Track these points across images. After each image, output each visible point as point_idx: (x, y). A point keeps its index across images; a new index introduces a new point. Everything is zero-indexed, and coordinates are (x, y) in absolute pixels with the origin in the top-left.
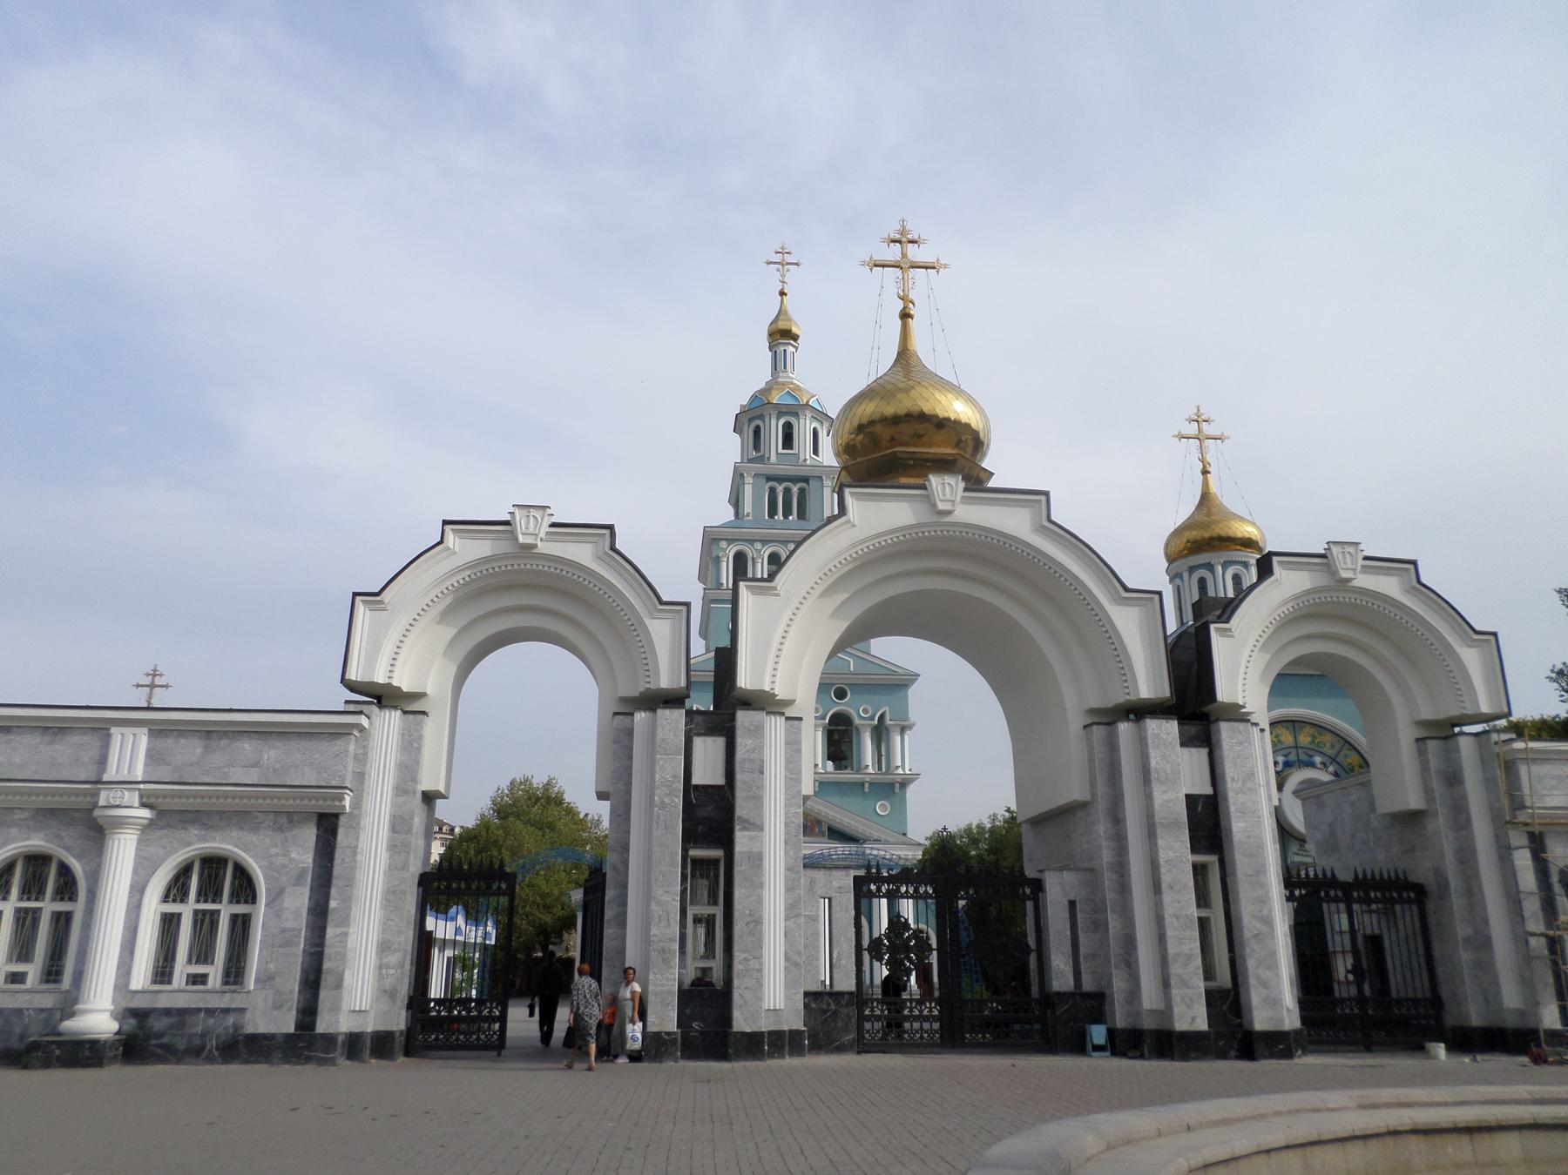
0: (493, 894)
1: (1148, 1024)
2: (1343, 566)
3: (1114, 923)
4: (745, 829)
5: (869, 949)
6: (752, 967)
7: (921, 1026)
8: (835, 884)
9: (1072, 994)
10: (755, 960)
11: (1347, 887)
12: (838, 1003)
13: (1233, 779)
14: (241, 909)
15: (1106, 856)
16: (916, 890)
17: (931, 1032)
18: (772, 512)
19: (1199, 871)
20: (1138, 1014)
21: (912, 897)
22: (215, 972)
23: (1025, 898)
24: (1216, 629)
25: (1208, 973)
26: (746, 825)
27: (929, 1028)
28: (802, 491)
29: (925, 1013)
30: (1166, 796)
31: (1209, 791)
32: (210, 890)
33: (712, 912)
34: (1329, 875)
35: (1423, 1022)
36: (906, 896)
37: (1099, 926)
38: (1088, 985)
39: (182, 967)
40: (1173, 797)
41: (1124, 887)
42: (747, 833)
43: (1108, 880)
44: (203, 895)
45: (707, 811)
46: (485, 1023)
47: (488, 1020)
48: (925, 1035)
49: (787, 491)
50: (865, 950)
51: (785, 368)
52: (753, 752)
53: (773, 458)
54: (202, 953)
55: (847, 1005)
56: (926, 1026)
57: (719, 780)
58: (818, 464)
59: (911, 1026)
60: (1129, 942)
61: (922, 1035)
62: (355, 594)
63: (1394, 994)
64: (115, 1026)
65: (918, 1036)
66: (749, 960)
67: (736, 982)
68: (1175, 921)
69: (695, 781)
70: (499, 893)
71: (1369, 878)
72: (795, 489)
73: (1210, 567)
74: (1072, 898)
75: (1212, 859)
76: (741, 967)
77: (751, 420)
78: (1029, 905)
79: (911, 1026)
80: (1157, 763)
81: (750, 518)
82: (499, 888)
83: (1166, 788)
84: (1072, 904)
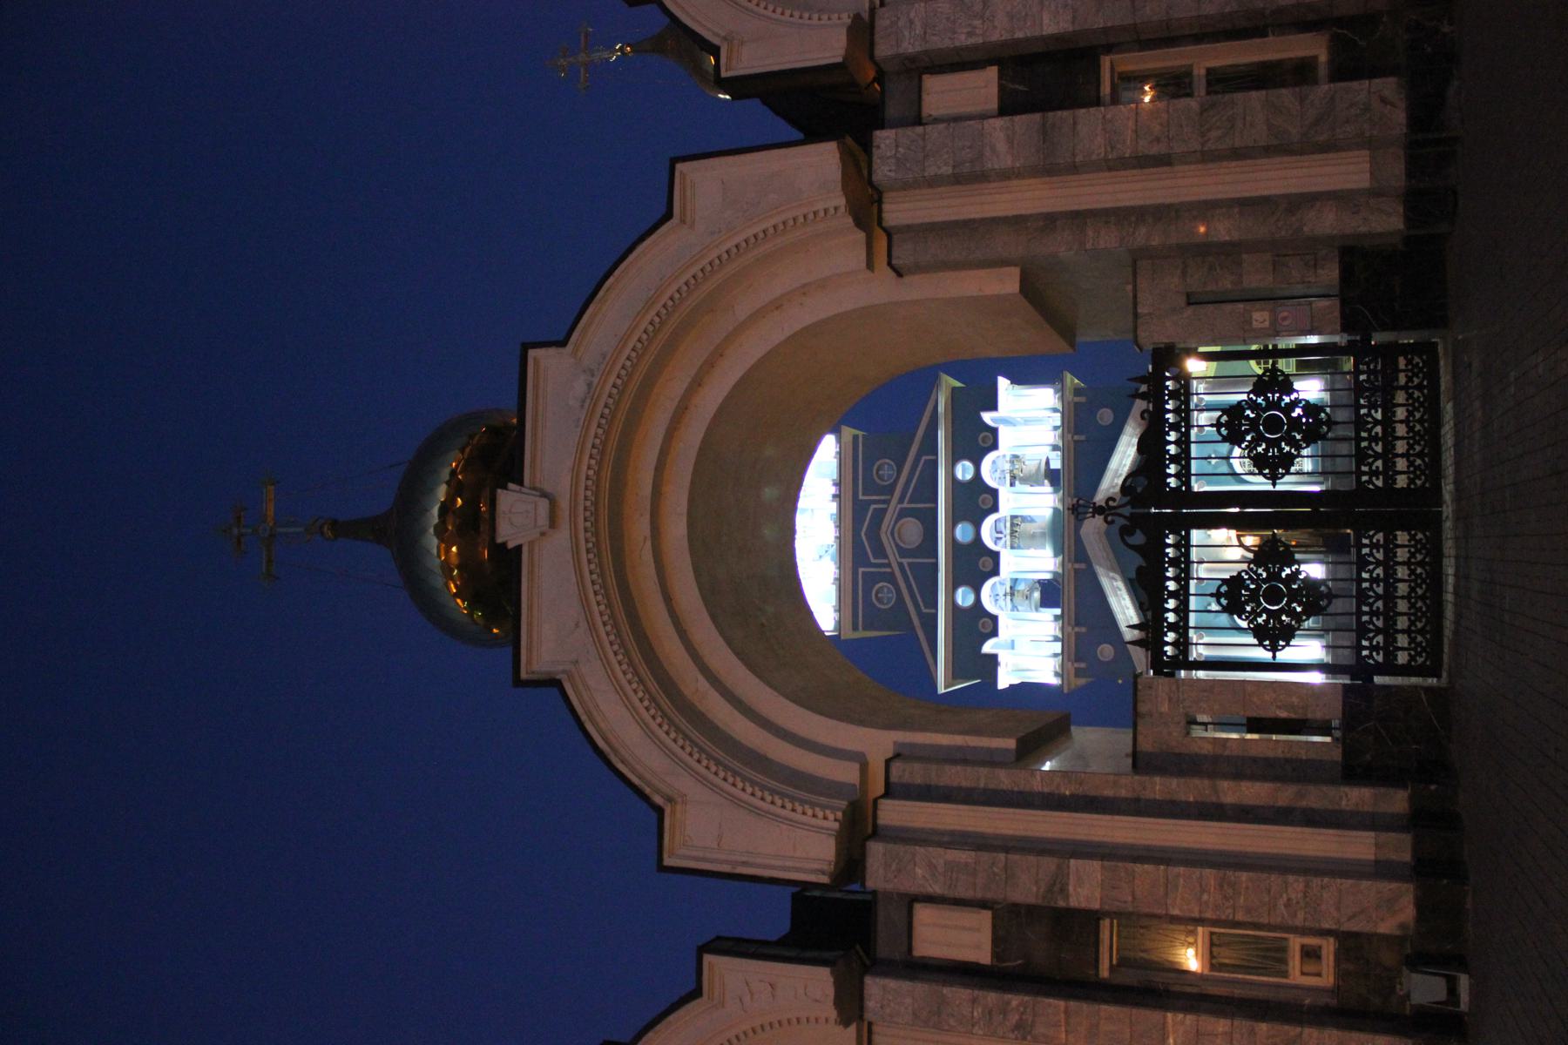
1: (1396, 171)
4: (1063, 890)
6: (1300, 895)
7: (1402, 456)
8: (1165, 708)
9: (1343, 303)
10: (1290, 890)
13: (970, 34)
15: (1107, 239)
17: (1416, 548)
20: (1375, 193)
24: (727, 70)
25: (1300, 73)
26: (1056, 889)
27: (1405, 618)
29: (1380, 623)
30: (1002, 147)
31: (992, 72)
35: (1402, 588)
37: (1229, 253)
38: (1330, 274)
40: (1002, 135)
42: (1071, 888)
43: (1145, 236)
46: (1396, 589)
47: (1392, 617)
48: (1416, 381)
50: (1274, 657)
52: (935, 867)
56: (1402, 555)
57: (986, 916)
59: (1402, 438)
61: (1415, 387)
65: (1417, 394)
66: (1289, 900)
68: (1214, 134)
71: (1128, 523)
74: (1182, 301)
76: (1301, 915)
79: (1402, 438)
80: (946, 164)
83: (988, 148)
84: (1192, 300)
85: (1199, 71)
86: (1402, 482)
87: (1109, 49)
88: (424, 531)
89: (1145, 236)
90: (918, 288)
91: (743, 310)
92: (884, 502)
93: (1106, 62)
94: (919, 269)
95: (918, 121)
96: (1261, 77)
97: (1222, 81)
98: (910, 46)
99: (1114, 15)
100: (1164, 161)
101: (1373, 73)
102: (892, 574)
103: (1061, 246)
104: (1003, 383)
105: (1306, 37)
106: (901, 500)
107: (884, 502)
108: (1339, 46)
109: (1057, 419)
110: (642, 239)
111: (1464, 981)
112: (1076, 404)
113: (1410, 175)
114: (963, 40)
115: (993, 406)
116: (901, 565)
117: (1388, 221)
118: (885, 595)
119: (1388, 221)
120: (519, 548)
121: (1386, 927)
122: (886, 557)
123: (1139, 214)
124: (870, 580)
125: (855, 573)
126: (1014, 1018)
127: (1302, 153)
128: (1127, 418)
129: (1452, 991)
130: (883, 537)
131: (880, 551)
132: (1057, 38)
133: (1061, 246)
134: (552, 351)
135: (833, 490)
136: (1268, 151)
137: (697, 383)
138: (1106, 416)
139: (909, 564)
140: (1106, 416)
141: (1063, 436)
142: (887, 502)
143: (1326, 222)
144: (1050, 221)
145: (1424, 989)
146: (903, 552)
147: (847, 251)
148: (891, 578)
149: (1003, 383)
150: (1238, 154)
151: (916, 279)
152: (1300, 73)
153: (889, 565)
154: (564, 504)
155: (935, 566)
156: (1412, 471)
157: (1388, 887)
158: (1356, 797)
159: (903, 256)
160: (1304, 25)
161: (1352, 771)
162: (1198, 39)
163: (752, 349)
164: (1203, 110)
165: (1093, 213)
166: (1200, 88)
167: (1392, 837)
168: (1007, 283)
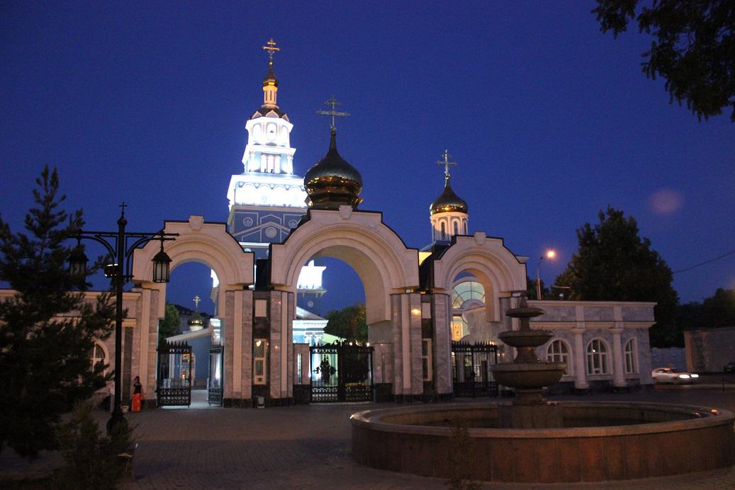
1: (406, 393)
3: (397, 361)
4: (274, 332)
11: (472, 347)
14: (604, 353)
15: (396, 339)
16: (175, 351)
17: (334, 397)
19: (424, 344)
20: (402, 389)
21: (174, 353)
22: (601, 369)
23: (368, 353)
32: (556, 350)
34: (185, 344)
35: (176, 398)
36: (172, 353)
37: (392, 362)
38: (387, 381)
39: (594, 370)
41: (401, 350)
43: (396, 345)
45: (260, 326)
54: (597, 365)
56: (333, 395)
60: (402, 366)
63: (489, 381)
64: (588, 385)
67: (271, 383)
69: (256, 315)
70: (186, 353)
75: (429, 340)
78: (369, 355)
85: (427, 357)
86: (314, 396)
87: (433, 340)
88: (335, 172)
89: (396, 345)
90: (388, 299)
91: (385, 260)
92: (282, 223)
93: (430, 340)
94: (392, 300)
95: (422, 302)
96: (425, 369)
97: (425, 361)
98: (437, 302)
99: (438, 342)
100: (411, 351)
101: (424, 390)
102: (256, 226)
103: (395, 330)
104: (324, 268)
105: (431, 377)
106: (283, 230)
107: (282, 223)
108: (429, 383)
109: (310, 288)
110: (402, 241)
111: (263, 407)
112: (315, 294)
113: (406, 395)
114: (436, 312)
115: (316, 264)
116: (259, 229)
117: (397, 392)
118: (248, 222)
119: (397, 392)
120: (338, 210)
121: (272, 393)
122: (263, 223)
123: (401, 346)
124: (254, 217)
125: (257, 211)
126: (247, 322)
127: (411, 376)
128: (310, 311)
129: (261, 405)
130: (270, 223)
131: (265, 221)
132: (435, 330)
133: (395, 330)
134: (380, 219)
135: (287, 205)
136: (411, 370)
137: (370, 248)
138: (311, 304)
139: (259, 233)
140: (311, 304)
141: (304, 290)
142: (282, 225)
143: (397, 380)
144: (400, 328)
145: (261, 400)
146: (264, 230)
147: (396, 283)
148: (254, 225)
149: (324, 268)
150: (411, 365)
151: (389, 299)
152: (425, 376)
153: (259, 225)
154: (349, 221)
155: (258, 242)
156: (315, 398)
157: (279, 393)
158: (291, 388)
159: (395, 297)
160: (434, 377)
161: (295, 386)
162: (433, 357)
163: (377, 262)
164: (420, 359)
165: (401, 336)
166: (424, 357)
167: (286, 394)
168: (388, 317)
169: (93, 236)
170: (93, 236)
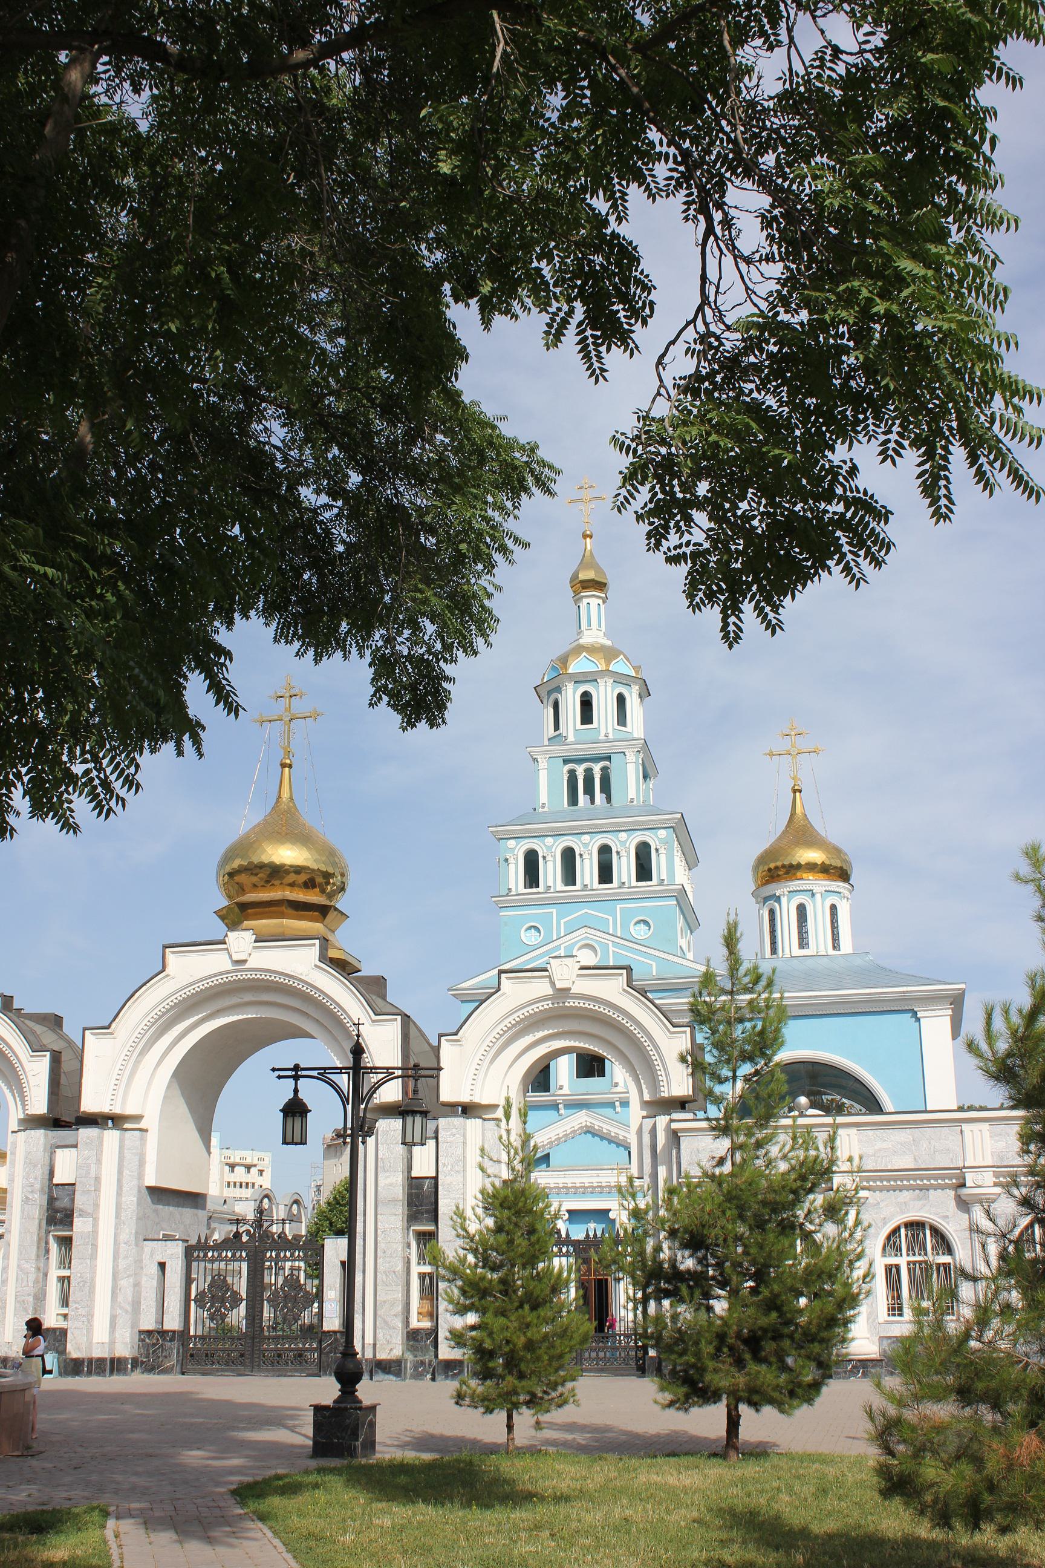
0: (237, 1260)
2: (560, 977)
5: (196, 1301)
8: (169, 1252)
12: (164, 1340)
18: (573, 800)
28: (605, 771)
30: (388, 1181)
33: (55, 1279)
44: (910, 1249)
49: (589, 774)
51: (589, 625)
53: (571, 738)
55: (170, 1341)
58: (628, 736)
62: (165, 947)
72: (597, 769)
73: (778, 899)
77: (549, 693)
81: (546, 809)
82: (198, 1256)
169: (315, 1073)
170: (315, 1073)
